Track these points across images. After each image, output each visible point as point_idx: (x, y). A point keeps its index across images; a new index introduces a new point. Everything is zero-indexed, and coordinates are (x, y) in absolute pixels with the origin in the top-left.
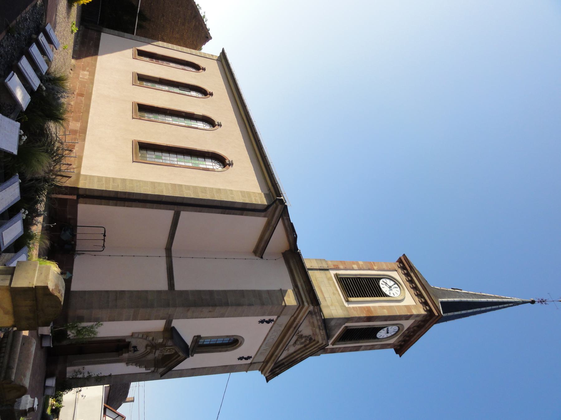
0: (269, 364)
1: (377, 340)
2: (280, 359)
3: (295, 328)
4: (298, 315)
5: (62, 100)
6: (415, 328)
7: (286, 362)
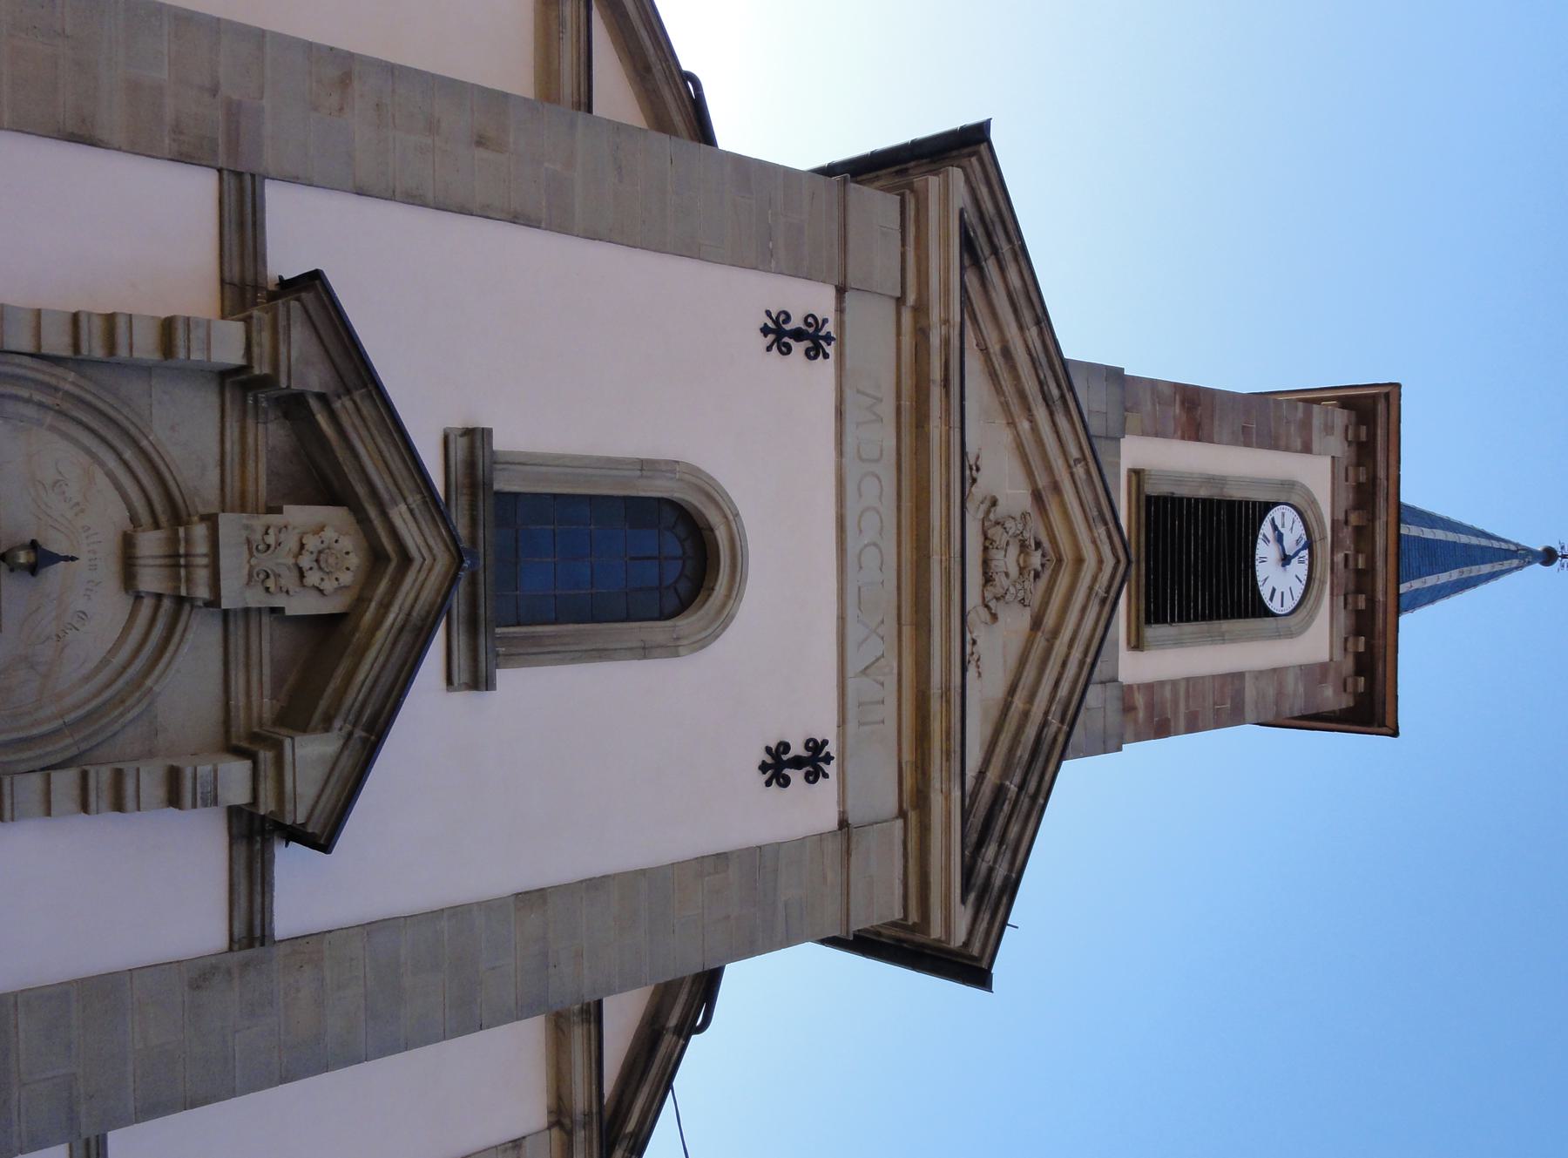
0: (937, 800)
1: (1267, 623)
5: (282, 432)
6: (1354, 519)
7: (1006, 771)
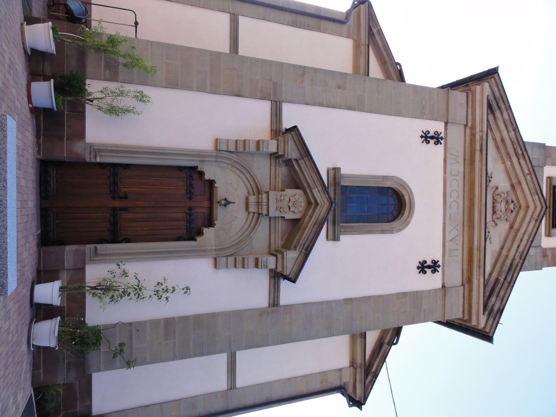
0: (475, 282)
2: (487, 274)
3: (481, 150)
4: (474, 119)
7: (500, 273)
